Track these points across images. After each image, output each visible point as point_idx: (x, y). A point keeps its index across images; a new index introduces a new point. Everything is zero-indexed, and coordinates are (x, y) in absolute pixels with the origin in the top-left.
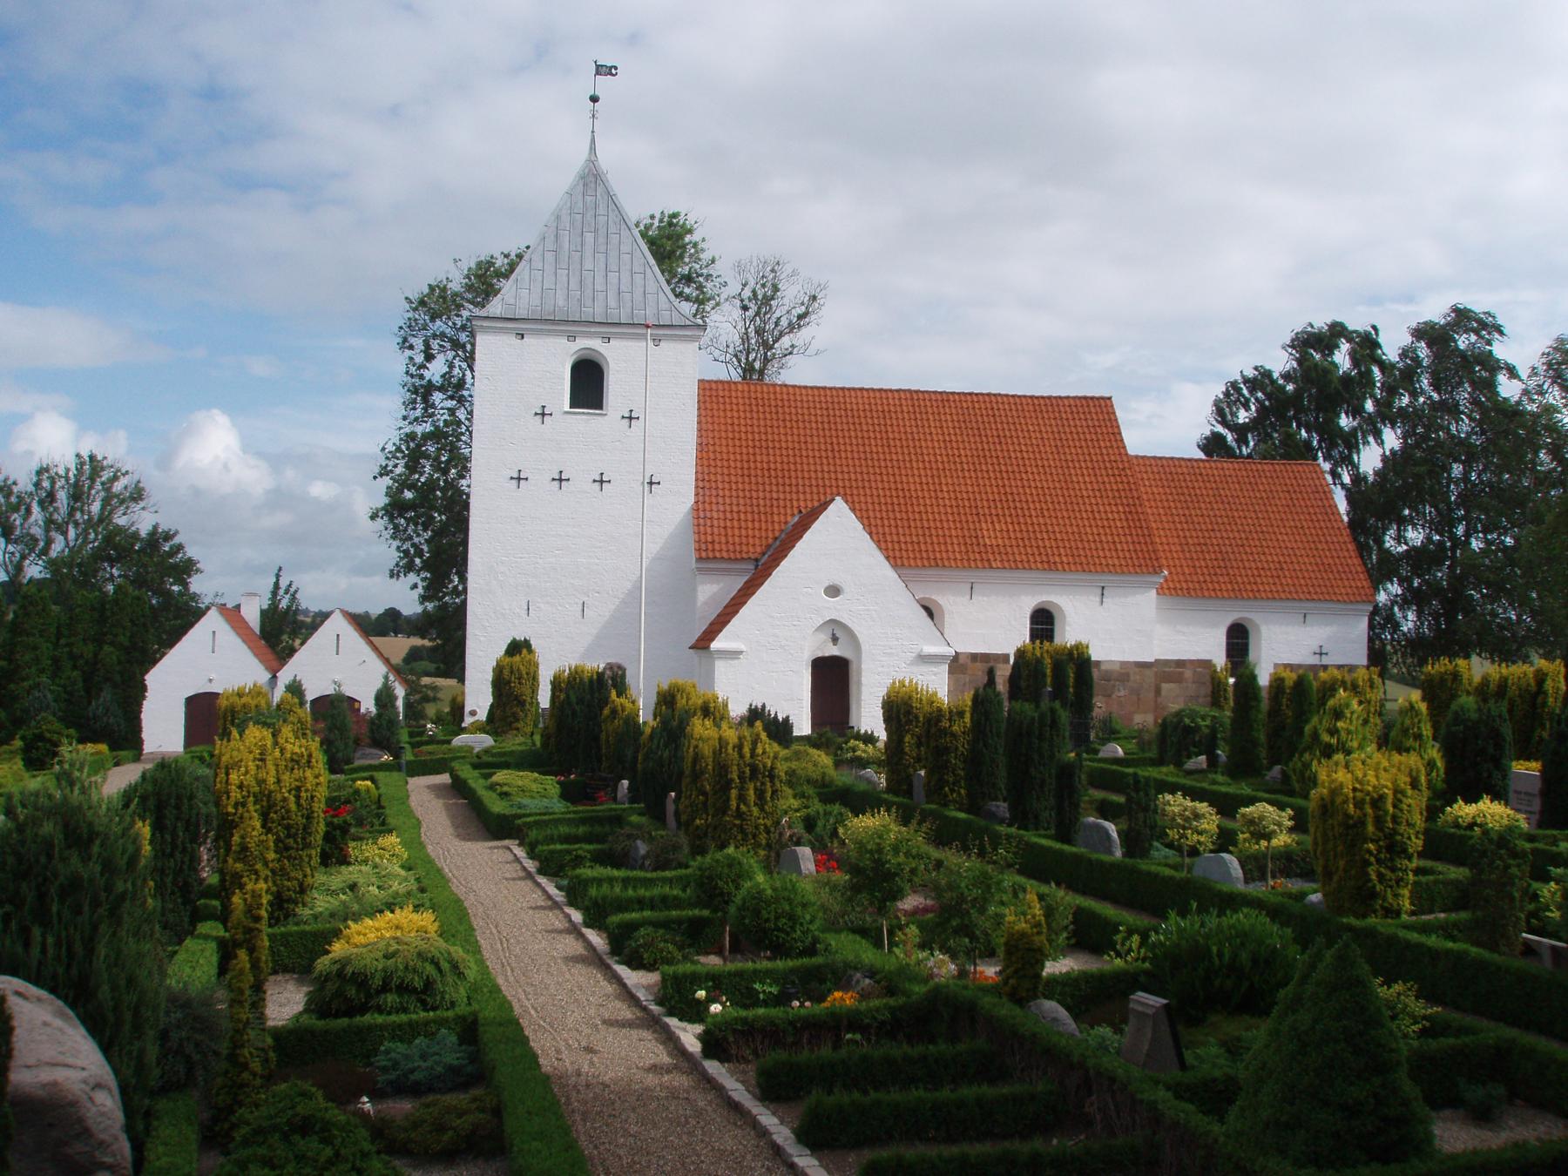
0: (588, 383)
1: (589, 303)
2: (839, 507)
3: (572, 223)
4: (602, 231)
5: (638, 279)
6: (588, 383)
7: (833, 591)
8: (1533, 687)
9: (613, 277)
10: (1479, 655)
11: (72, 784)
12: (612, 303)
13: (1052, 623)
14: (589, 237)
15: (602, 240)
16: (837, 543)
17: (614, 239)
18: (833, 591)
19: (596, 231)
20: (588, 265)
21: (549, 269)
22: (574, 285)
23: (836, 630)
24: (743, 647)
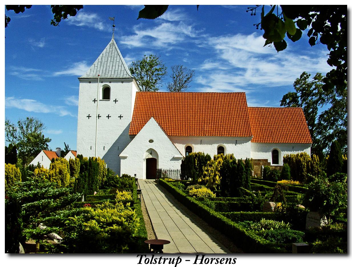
0: (106, 94)
1: (107, 74)
2: (152, 119)
3: (106, 55)
4: (113, 57)
5: (120, 67)
6: (106, 94)
7: (151, 141)
8: (218, 57)
9: (114, 67)
10: (196, 80)
11: (14, 185)
12: (113, 73)
13: (224, 150)
14: (109, 58)
15: (112, 59)
16: (152, 128)
17: (115, 58)
18: (151, 141)
19: (111, 57)
20: (108, 65)
21: (99, 66)
22: (104, 69)
23: (151, 151)
24: (128, 156)
